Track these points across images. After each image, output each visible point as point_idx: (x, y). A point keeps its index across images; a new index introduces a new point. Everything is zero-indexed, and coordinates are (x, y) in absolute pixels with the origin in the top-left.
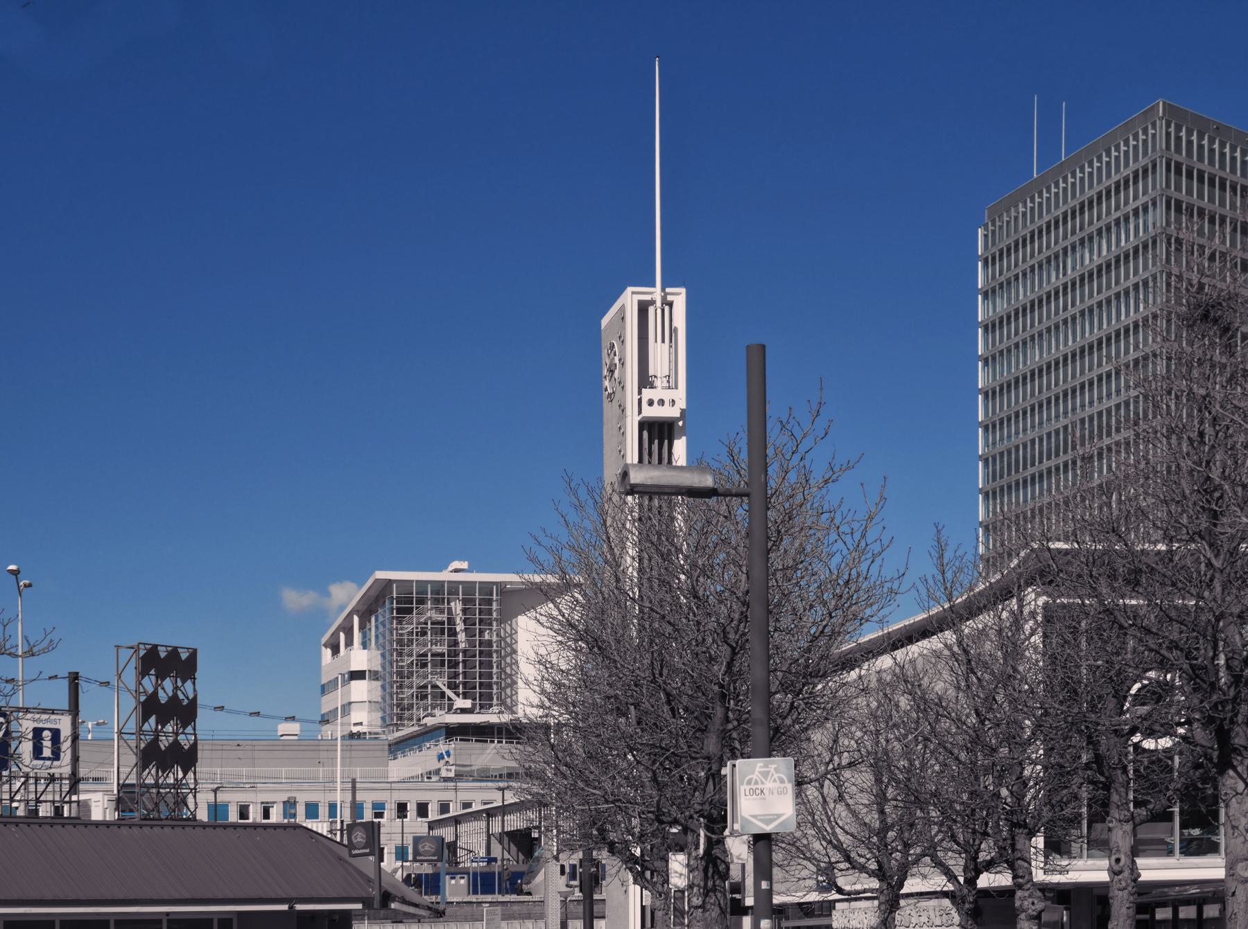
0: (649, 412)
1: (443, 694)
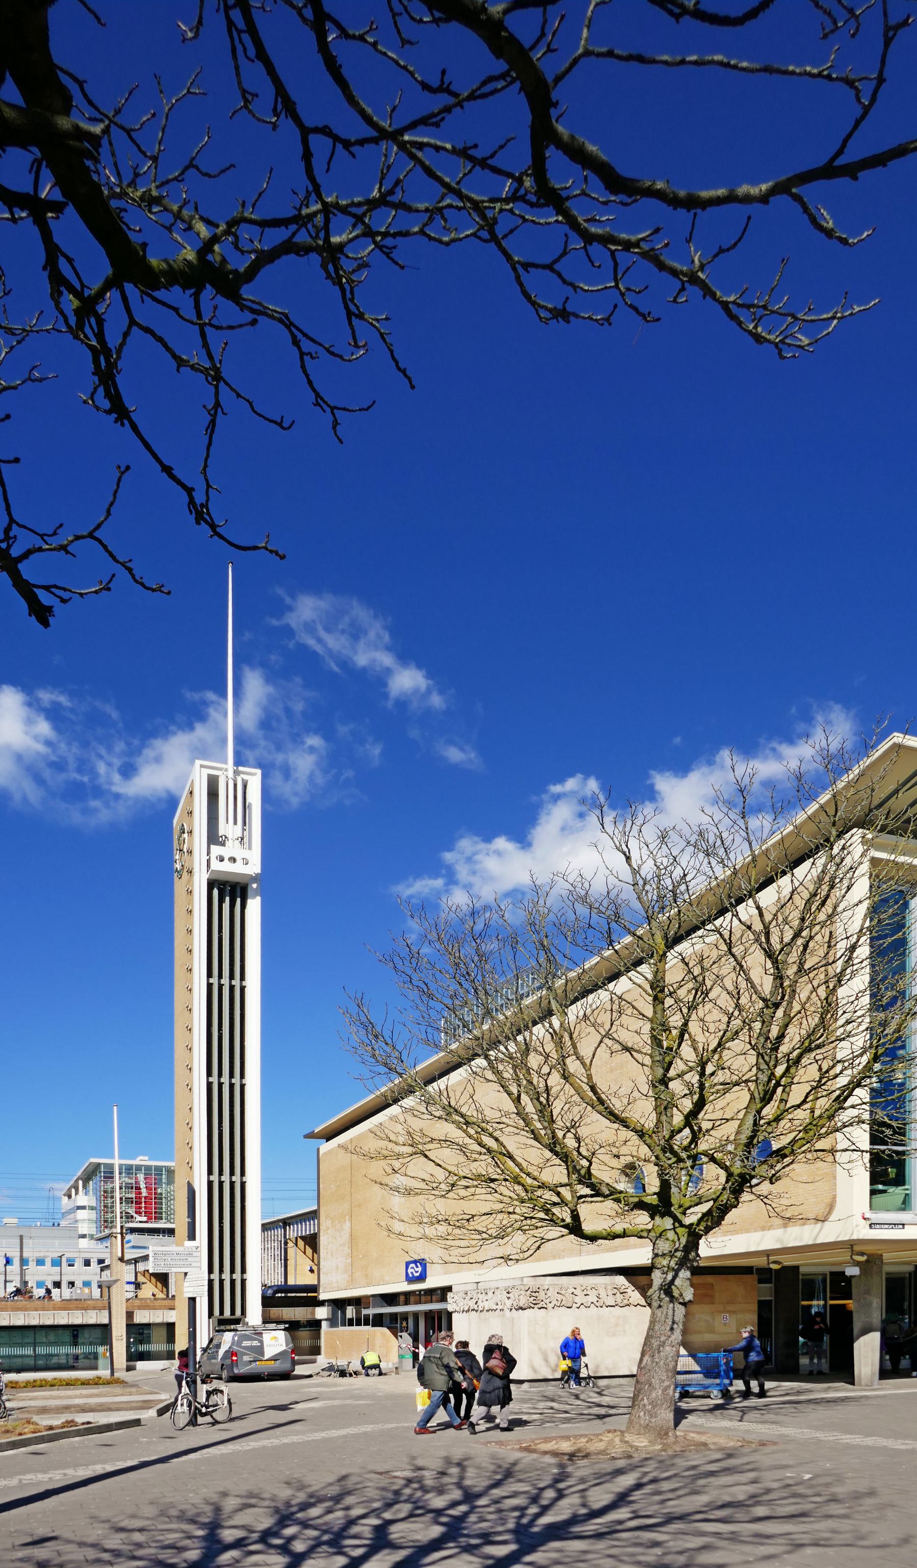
0: (216, 866)
1: (132, 1217)
